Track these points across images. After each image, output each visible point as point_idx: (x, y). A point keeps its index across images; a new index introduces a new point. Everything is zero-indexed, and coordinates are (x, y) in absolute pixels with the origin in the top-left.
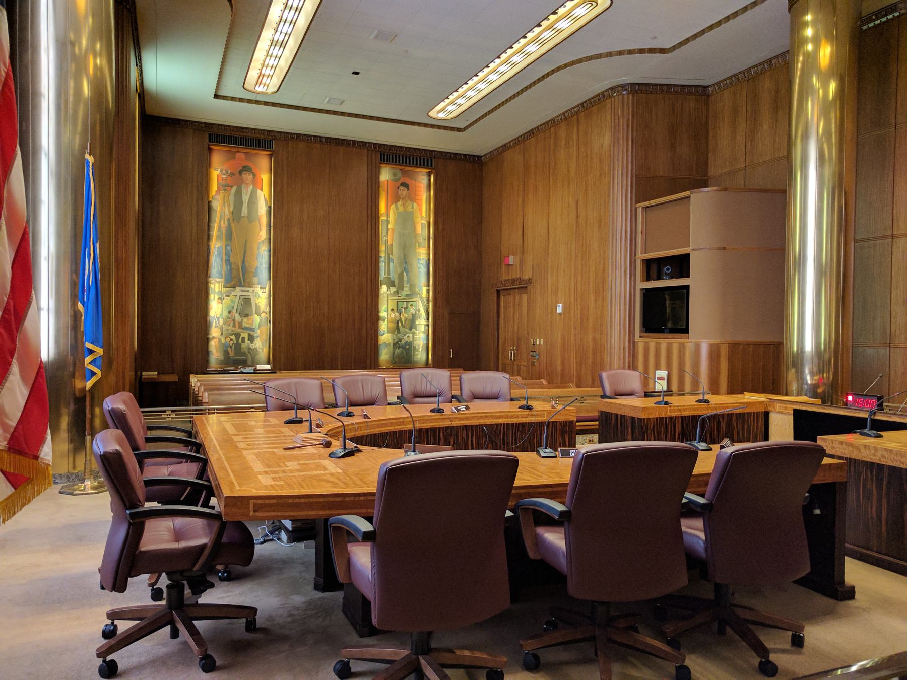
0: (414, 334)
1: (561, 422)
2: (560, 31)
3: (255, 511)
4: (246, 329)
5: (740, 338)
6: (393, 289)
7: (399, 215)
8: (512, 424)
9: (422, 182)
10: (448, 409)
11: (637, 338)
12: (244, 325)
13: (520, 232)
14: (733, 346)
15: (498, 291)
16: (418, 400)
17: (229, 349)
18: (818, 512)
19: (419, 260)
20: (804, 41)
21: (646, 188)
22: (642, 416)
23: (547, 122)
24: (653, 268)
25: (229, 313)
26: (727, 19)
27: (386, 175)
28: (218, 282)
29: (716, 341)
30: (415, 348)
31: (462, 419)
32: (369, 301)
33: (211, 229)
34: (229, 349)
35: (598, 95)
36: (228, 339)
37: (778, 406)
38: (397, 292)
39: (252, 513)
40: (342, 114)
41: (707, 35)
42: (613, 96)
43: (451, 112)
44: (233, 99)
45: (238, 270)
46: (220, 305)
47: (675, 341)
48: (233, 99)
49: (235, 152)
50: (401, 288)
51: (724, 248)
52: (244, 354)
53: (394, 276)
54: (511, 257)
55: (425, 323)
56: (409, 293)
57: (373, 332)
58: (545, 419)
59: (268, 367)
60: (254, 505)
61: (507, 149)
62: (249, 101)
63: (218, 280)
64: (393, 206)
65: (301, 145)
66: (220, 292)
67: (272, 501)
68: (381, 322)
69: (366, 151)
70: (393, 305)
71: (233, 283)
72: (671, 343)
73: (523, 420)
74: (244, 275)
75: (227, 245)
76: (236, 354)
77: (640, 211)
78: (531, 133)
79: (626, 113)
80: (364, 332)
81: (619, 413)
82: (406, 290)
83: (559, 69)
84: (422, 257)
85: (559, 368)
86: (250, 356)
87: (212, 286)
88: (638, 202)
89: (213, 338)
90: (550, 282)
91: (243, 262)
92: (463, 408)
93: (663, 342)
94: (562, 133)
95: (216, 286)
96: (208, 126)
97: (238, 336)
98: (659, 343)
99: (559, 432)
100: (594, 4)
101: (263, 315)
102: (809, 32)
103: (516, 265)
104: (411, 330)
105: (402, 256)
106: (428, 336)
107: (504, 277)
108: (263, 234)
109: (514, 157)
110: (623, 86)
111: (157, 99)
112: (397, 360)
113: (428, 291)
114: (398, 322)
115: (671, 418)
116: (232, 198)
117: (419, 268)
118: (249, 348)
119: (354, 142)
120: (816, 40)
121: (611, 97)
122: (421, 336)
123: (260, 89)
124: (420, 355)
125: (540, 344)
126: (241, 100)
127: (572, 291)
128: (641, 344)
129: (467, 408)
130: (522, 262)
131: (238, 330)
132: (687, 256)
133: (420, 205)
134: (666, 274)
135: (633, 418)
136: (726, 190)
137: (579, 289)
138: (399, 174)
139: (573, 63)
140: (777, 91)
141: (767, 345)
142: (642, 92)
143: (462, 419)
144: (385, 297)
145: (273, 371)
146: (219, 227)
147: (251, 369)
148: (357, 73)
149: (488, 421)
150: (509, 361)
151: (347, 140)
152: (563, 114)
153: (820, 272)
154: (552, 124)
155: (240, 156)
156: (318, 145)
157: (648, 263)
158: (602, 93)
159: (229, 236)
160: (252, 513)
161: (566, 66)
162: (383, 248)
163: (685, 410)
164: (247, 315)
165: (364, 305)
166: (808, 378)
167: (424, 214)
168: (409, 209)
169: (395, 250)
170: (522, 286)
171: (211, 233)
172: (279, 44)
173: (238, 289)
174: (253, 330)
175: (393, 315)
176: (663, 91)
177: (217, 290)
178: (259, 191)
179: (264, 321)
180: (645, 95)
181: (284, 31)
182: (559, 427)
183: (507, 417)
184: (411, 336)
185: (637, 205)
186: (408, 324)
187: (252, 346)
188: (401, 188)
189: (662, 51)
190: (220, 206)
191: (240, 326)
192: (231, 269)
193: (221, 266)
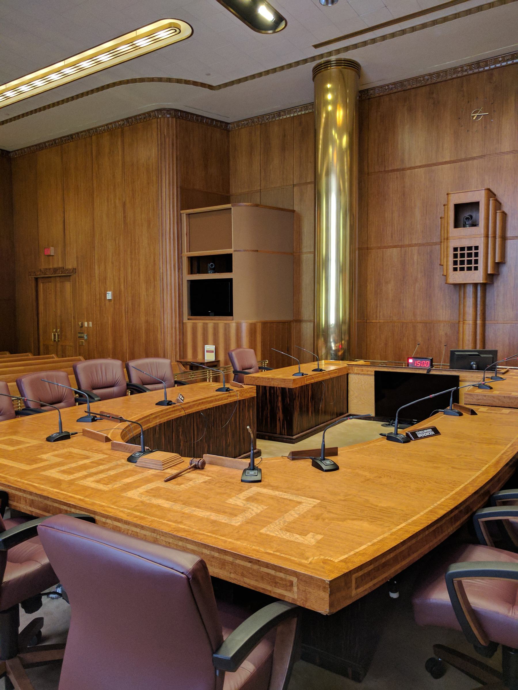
2: (137, 48)
5: (267, 319)
11: (185, 320)
13: (61, 226)
14: (264, 324)
15: (36, 279)
20: (326, 103)
21: (189, 198)
23: (88, 130)
24: (197, 264)
26: (267, 72)
29: (253, 321)
35: (144, 114)
37: (356, 370)
41: (249, 82)
42: (158, 118)
47: (221, 322)
51: (257, 251)
54: (52, 249)
61: (42, 149)
72: (207, 324)
78: (70, 137)
79: (171, 133)
81: (268, 385)
83: (121, 83)
85: (110, 346)
88: (182, 209)
90: (97, 272)
93: (210, 322)
94: (106, 140)
98: (207, 324)
102: (329, 97)
103: (54, 257)
107: (43, 266)
110: (169, 111)
120: (334, 103)
127: (122, 280)
128: (189, 324)
130: (64, 254)
132: (231, 255)
134: (211, 269)
136: (257, 205)
137: (129, 278)
139: (134, 81)
140: (284, 136)
141: (284, 323)
142: (184, 119)
150: (52, 343)
152: (107, 125)
153: (340, 270)
157: (191, 259)
166: (333, 345)
170: (65, 275)
176: (198, 120)
185: (182, 212)
189: (210, 87)
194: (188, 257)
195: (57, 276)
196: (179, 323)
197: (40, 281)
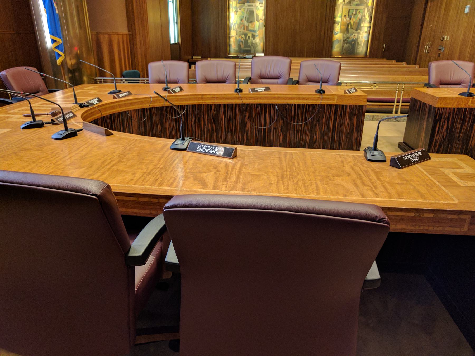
0: (359, 33)
4: (251, 31)
10: (247, 88)
12: (250, 28)
16: (263, 80)
17: (241, 43)
22: (438, 106)
25: (241, 20)
30: (358, 44)
31: (257, 98)
34: (241, 43)
52: (249, 46)
55: (368, 25)
56: (358, 2)
57: (329, 32)
58: (334, 102)
66: (236, 7)
70: (345, 12)
73: (314, 102)
76: (245, 47)
80: (323, 32)
81: (423, 101)
87: (231, 3)
89: (232, 37)
92: (178, 90)
97: (246, 35)
99: (348, 115)
101: (261, 22)
104: (357, 30)
106: (369, 35)
114: (348, 24)
118: (252, 43)
122: (363, 35)
124: (362, 49)
125: (447, 40)
129: (267, 89)
135: (430, 106)
143: (257, 98)
144: (341, 6)
147: (251, 56)
149: (215, 102)
163: (105, 109)
173: (246, 4)
174: (255, 31)
175: (345, 20)
177: (234, 6)
179: (261, 26)
182: (348, 111)
183: (299, 98)
184: (356, 35)
186: (355, 27)
187: (254, 41)
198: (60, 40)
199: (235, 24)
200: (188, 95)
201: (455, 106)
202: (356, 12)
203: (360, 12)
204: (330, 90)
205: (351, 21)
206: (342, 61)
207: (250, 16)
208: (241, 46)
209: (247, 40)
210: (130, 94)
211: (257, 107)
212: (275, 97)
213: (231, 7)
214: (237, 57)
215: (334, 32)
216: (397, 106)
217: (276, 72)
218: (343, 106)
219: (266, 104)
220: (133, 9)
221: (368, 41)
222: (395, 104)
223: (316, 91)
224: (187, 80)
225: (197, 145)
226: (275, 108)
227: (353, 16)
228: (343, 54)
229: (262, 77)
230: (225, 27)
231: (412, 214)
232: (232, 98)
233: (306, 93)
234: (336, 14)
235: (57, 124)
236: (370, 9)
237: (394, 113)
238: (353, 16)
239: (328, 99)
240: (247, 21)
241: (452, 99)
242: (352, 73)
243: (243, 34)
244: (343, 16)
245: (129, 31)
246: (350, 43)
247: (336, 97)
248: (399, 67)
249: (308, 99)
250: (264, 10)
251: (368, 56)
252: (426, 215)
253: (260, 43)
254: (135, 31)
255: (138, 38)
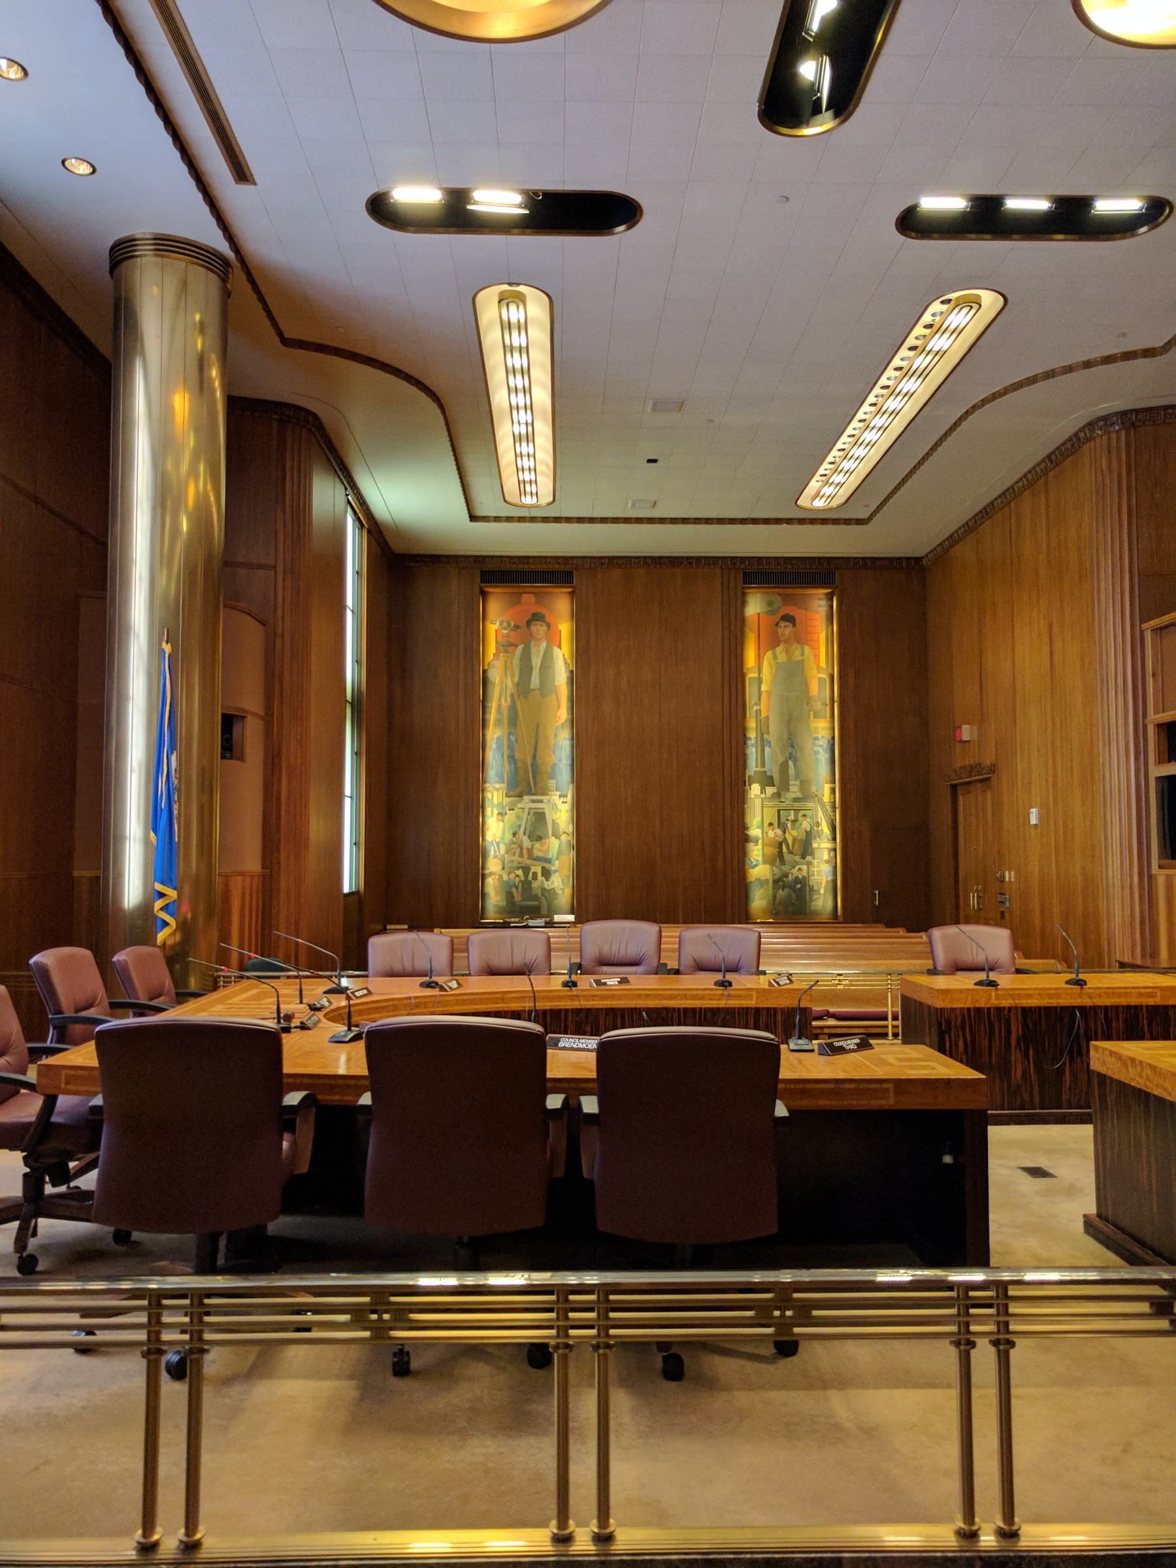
0: (809, 864)
1: (783, 1010)
3: (67, 1083)
4: (538, 859)
6: (770, 790)
7: (779, 667)
8: (694, 1009)
9: (819, 610)
12: (536, 853)
13: (977, 687)
16: (605, 969)
17: (514, 890)
18: (948, 1159)
19: (816, 739)
25: (514, 834)
27: (755, 606)
28: (498, 790)
30: (812, 889)
32: (728, 811)
33: (488, 711)
34: (514, 890)
35: (1070, 439)
36: (512, 876)
38: (778, 795)
39: (63, 1086)
40: (662, 521)
43: (832, 497)
44: (497, 519)
45: (527, 772)
46: (501, 824)
48: (497, 519)
49: (521, 594)
50: (784, 786)
52: (536, 898)
53: (773, 769)
56: (799, 795)
57: (736, 861)
58: (752, 1003)
59: (571, 918)
60: (66, 1075)
61: (952, 546)
62: (521, 519)
63: (497, 786)
64: (769, 654)
65: (616, 573)
66: (500, 805)
67: (84, 1073)
68: (751, 845)
69: (718, 571)
70: (770, 815)
71: (519, 789)
73: (714, 1004)
74: (534, 778)
75: (510, 733)
77: (1148, 635)
78: (986, 513)
80: (720, 863)
82: (794, 791)
84: (821, 734)
86: (543, 899)
87: (489, 795)
89: (491, 874)
91: (534, 757)
92: (454, 984)
95: (495, 795)
96: (479, 559)
97: (526, 870)
100: (976, 306)
104: (803, 857)
105: (785, 737)
106: (835, 867)
107: (958, 762)
108: (563, 714)
109: (964, 552)
110: (1106, 420)
111: (399, 531)
112: (780, 908)
113: (833, 791)
114: (780, 844)
115: (999, 1010)
116: (516, 662)
117: (817, 753)
118: (544, 889)
119: (698, 559)
121: (1088, 440)
122: (822, 868)
123: (528, 500)
124: (823, 901)
125: (1010, 881)
126: (509, 519)
128: (1161, 876)
129: (624, 981)
131: (527, 861)
133: (815, 649)
135: (929, 1007)
138: (778, 600)
139: (994, 397)
144: (758, 803)
145: (579, 921)
146: (499, 706)
147: (540, 922)
148: (655, 461)
151: (688, 558)
154: (1010, 495)
155: (528, 598)
156: (643, 571)
158: (1076, 435)
159: (513, 720)
160: (63, 1086)
161: (984, 402)
162: (752, 724)
163: (1029, 996)
164: (539, 838)
165: (720, 817)
167: (823, 663)
168: (797, 655)
169: (773, 727)
171: (487, 716)
172: (524, 438)
173: (526, 798)
174: (548, 861)
175: (771, 834)
177: (495, 802)
178: (556, 649)
179: (565, 847)
180: (1150, 428)
181: (523, 421)
182: (779, 1018)
183: (685, 997)
184: (804, 867)
185: (1144, 626)
186: (797, 848)
187: (548, 885)
188: (783, 624)
189: (1148, 353)
190: (501, 678)
191: (530, 855)
192: (516, 769)
193: (503, 765)
194: (1159, 726)
195: (977, 781)
196: (1141, 875)
197: (960, 790)
198: (173, 894)
199: (498, 844)
200: (478, 994)
201: (969, 1005)
202: (796, 815)
203: (804, 815)
204: (741, 981)
205: (787, 835)
206: (766, 932)
207: (538, 825)
208: (513, 897)
209: (530, 883)
210: (370, 993)
211: (607, 1014)
212: (640, 995)
213: (487, 804)
214: (505, 925)
215: (747, 862)
216: (893, 1027)
217: (631, 952)
218: (768, 1009)
219: (624, 1009)
220: (278, 818)
221: (835, 881)
222: (890, 1023)
223: (716, 984)
224: (448, 971)
225: (558, 1040)
226: (641, 1015)
227: (789, 825)
228: (777, 914)
229: (604, 962)
230: (475, 851)
231: (831, 1086)
232: (559, 998)
233: (699, 989)
234: (748, 820)
235: (308, 1029)
236: (829, 809)
237: (890, 1037)
238: (789, 825)
239: (739, 997)
240: (529, 837)
241: (961, 991)
242: (801, 958)
243: (518, 868)
244: (766, 825)
245: (263, 868)
246: (792, 887)
247: (754, 993)
248: (908, 943)
249: (702, 998)
250: (572, 810)
251: (841, 920)
252: (847, 1086)
253: (563, 890)
254: (279, 868)
255: (284, 883)
